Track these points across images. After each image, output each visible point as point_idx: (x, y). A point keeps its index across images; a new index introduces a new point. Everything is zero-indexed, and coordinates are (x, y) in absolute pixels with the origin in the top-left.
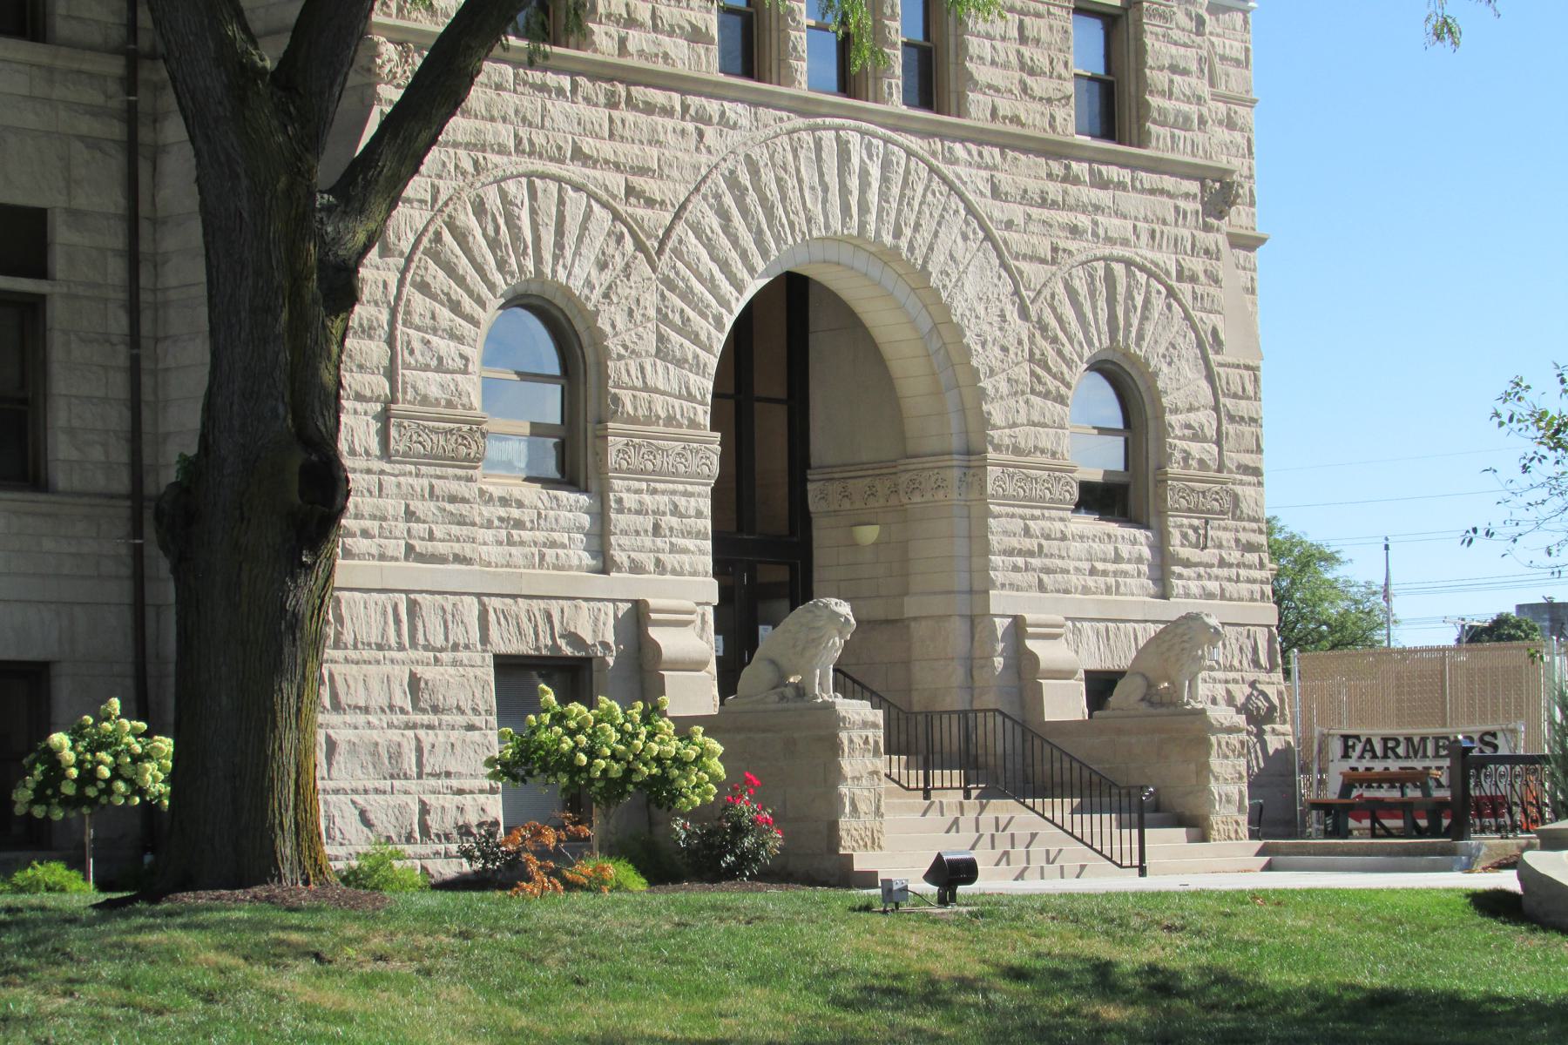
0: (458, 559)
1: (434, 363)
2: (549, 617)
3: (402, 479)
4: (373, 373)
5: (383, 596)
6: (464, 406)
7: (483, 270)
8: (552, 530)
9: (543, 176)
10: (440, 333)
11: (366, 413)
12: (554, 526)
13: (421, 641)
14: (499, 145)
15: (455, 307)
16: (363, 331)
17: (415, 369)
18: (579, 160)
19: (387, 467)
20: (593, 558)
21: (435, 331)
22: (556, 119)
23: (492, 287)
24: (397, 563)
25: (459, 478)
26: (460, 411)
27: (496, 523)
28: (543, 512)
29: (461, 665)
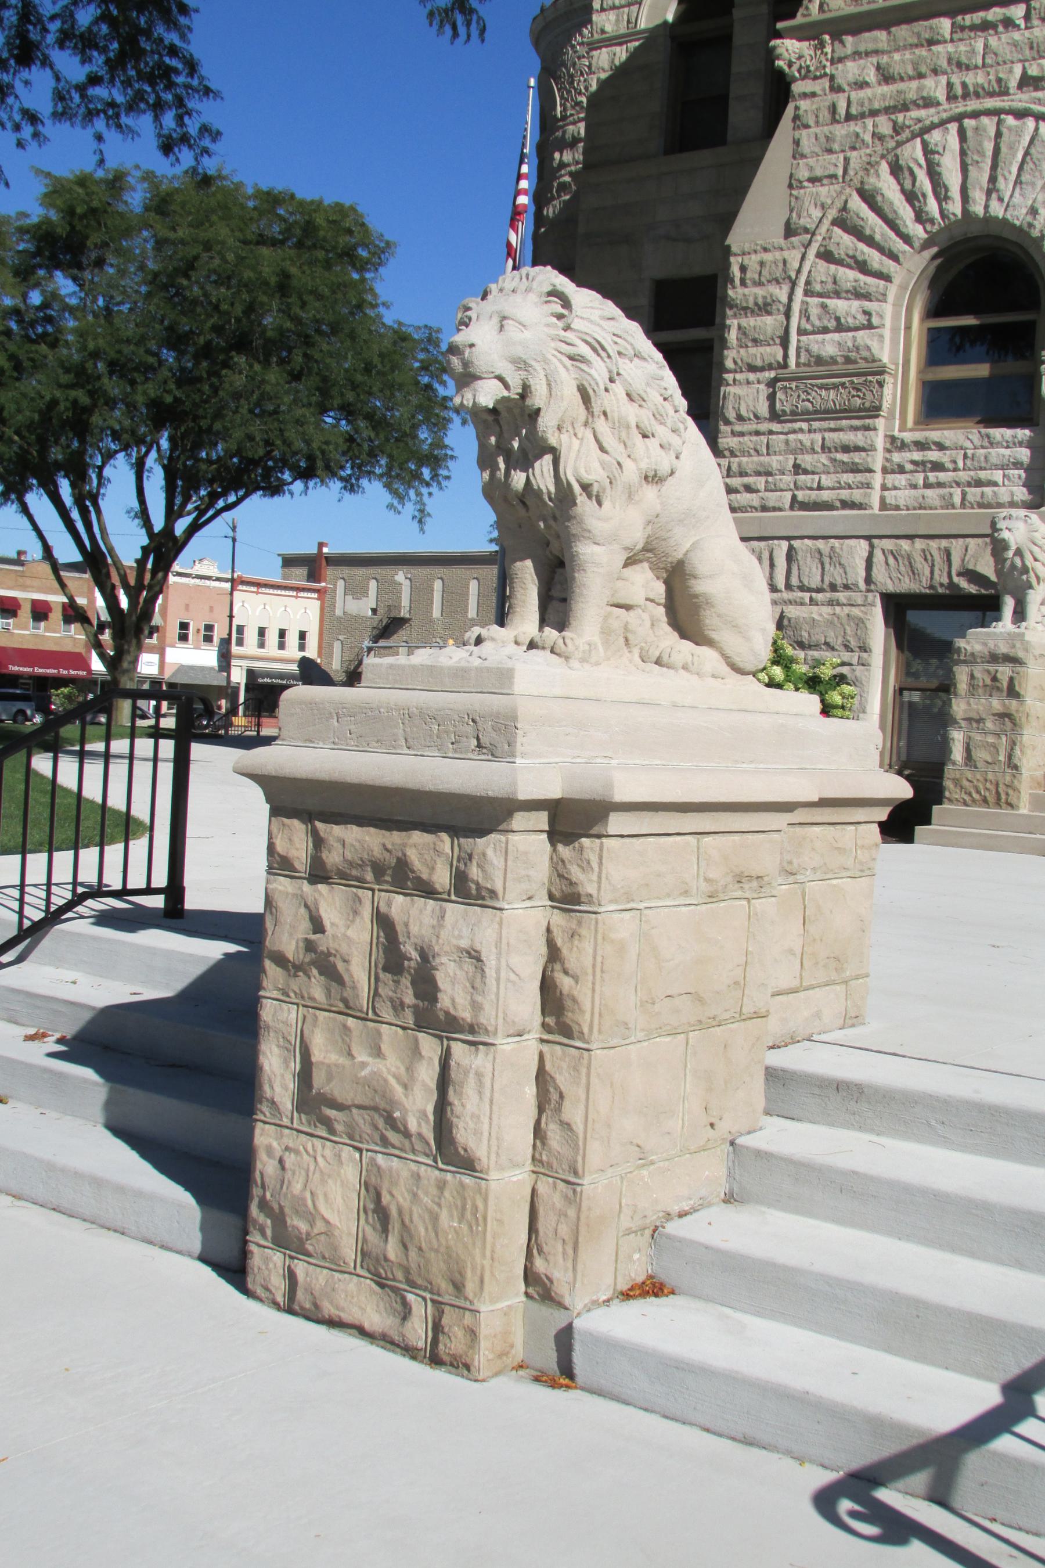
0: (846, 505)
1: (832, 324)
2: (948, 553)
3: (791, 437)
4: (769, 345)
5: (763, 544)
6: (865, 359)
7: (897, 225)
8: (981, 469)
9: (975, 115)
10: (844, 295)
11: (759, 382)
12: (983, 465)
13: (794, 581)
14: (923, 98)
15: (863, 267)
16: (760, 309)
17: (813, 333)
18: (1028, 85)
19: (775, 427)
20: (1030, 493)
21: (837, 294)
22: (1000, 51)
23: (906, 239)
24: (835, 513)
25: (856, 429)
26: (862, 364)
27: (909, 467)
28: (970, 453)
29: (838, 604)
